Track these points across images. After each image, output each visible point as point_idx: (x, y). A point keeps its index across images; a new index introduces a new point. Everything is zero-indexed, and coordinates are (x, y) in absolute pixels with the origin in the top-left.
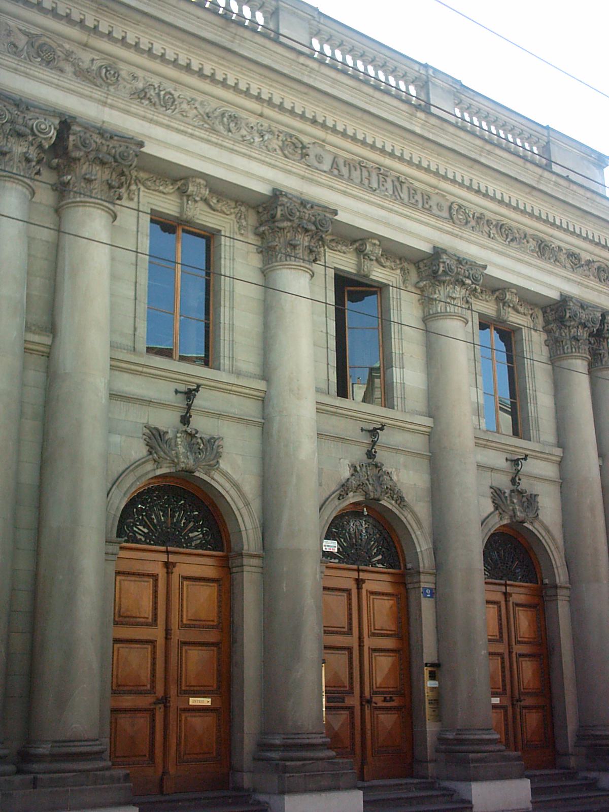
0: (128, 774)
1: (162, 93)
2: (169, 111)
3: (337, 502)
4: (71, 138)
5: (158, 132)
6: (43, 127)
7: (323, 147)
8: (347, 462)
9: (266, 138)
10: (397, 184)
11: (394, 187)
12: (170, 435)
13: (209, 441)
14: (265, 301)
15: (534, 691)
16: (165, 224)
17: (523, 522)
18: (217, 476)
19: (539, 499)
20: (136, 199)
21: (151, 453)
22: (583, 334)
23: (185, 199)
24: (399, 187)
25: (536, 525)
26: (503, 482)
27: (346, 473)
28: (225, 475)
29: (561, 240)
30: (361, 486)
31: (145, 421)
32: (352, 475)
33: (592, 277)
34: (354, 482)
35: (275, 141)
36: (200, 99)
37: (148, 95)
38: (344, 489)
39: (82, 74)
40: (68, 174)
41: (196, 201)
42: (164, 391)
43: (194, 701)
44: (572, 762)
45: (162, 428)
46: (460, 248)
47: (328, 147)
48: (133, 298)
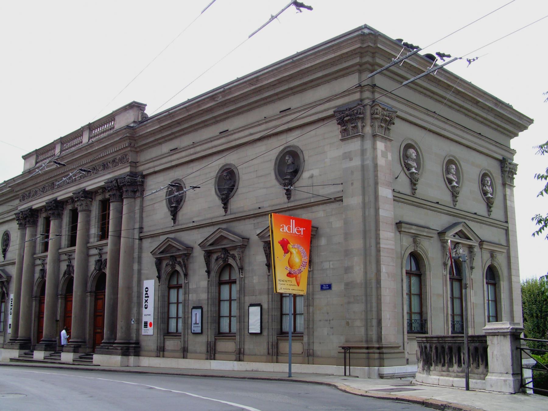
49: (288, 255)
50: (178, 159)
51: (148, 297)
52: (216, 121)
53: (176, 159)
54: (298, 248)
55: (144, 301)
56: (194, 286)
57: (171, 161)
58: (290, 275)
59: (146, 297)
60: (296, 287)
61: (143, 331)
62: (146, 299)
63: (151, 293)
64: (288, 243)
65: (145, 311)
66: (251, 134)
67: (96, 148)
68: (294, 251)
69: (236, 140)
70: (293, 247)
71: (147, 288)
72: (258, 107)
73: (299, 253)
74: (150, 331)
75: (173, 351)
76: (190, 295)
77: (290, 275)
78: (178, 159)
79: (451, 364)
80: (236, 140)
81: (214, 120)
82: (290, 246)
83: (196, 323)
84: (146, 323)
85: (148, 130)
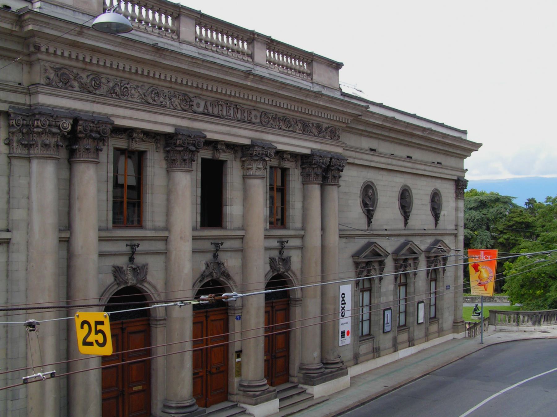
0: (54, 373)
1: (122, 88)
2: (125, 97)
3: (199, 284)
4: (79, 128)
5: (120, 112)
6: (65, 125)
7: (200, 98)
8: (204, 262)
9: (172, 100)
10: (235, 109)
11: (234, 111)
12: (125, 268)
13: (142, 267)
14: (168, 186)
15: (164, 53)
16: (119, 152)
17: (284, 273)
18: (146, 284)
19: (292, 259)
20: (106, 144)
21: (115, 280)
22: (319, 171)
23: (131, 140)
24: (236, 111)
25: (289, 272)
26: (275, 254)
27: (203, 268)
28: (150, 283)
29: (313, 120)
30: (211, 274)
31: (112, 264)
32: (206, 268)
33: (327, 137)
34: (207, 273)
35: (177, 100)
36: (140, 85)
37: (116, 91)
38: (203, 276)
39: (84, 88)
40: (77, 145)
41: (136, 141)
42: (122, 247)
43: (135, 389)
44: (295, 380)
45: (120, 266)
46: (264, 138)
47: (203, 97)
48: (106, 200)
49: (478, 273)
50: (377, 162)
51: (345, 303)
52: (409, 145)
53: (376, 161)
54: (486, 268)
55: (341, 309)
56: (384, 290)
57: (371, 161)
58: (480, 284)
59: (342, 304)
60: (485, 292)
61: (340, 342)
62: (343, 306)
63: (348, 299)
64: (478, 265)
65: (342, 321)
66: (425, 170)
67: (321, 103)
68: (483, 270)
69: (417, 169)
70: (482, 268)
71: (343, 294)
72: (429, 150)
73: (487, 271)
74: (348, 340)
75: (365, 354)
76: (382, 298)
77: (480, 284)
78: (377, 162)
79: (551, 320)
80: (417, 169)
81: (407, 143)
82: (480, 268)
83: (387, 323)
84: (343, 333)
85: (371, 120)
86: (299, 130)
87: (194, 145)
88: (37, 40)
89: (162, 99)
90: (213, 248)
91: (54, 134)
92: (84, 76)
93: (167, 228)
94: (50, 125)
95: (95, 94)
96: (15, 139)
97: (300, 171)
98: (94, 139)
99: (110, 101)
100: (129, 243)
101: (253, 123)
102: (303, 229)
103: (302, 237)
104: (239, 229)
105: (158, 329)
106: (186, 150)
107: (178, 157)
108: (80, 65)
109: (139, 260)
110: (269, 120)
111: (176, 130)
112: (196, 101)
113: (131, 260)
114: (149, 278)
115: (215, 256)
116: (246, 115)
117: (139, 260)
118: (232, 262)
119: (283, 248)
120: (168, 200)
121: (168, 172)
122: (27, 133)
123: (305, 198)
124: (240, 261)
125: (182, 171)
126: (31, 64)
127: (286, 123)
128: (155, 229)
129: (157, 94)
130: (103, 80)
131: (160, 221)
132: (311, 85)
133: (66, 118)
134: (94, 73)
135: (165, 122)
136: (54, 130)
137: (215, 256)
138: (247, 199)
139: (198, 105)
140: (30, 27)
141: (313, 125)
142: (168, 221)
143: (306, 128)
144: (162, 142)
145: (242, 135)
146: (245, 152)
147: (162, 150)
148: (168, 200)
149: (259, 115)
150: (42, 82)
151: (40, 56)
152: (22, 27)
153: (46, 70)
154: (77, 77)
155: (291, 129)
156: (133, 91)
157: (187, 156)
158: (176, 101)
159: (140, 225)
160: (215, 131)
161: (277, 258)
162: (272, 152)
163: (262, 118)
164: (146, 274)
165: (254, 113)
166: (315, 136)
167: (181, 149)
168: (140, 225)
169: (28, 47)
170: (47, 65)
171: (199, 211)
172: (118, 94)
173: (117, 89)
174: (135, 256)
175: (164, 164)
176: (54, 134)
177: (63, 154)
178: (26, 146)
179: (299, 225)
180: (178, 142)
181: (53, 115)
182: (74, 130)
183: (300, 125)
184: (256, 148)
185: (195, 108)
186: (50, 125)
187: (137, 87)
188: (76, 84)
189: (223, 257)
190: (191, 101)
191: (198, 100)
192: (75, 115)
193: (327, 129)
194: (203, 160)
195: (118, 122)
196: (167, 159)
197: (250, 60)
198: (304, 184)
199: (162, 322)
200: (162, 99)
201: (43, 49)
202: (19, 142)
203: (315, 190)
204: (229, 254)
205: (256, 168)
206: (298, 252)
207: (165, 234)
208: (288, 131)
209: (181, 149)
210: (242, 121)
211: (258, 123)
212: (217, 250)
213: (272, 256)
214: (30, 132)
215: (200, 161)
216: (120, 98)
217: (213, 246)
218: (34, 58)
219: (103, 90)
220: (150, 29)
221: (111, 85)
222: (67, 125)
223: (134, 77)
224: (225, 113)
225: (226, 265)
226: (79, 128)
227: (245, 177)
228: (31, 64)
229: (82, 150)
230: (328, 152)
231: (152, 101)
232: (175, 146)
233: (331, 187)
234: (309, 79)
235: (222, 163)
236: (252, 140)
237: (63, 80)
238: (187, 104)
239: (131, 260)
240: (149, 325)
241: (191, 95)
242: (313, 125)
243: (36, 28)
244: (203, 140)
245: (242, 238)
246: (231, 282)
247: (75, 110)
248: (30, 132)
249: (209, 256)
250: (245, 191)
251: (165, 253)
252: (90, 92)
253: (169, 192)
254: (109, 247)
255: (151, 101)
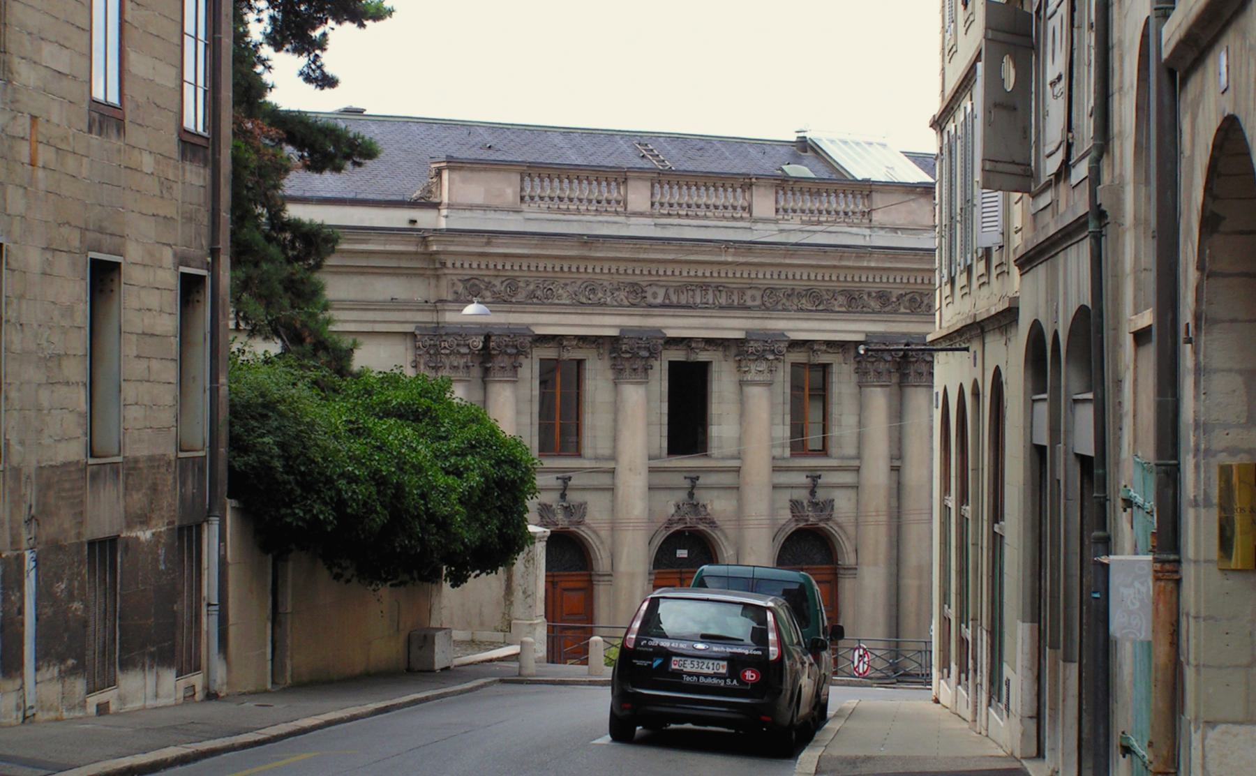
11: (715, 295)
28: (589, 528)
33: (902, 310)
34: (676, 518)
38: (670, 522)
42: (802, 479)
86: (841, 306)
87: (648, 349)
88: (442, 257)
89: (600, 295)
90: (687, 483)
91: (463, 355)
92: (497, 282)
93: (613, 458)
94: (458, 345)
95: (511, 302)
96: (422, 361)
97: (854, 366)
98: (510, 355)
99: (529, 308)
100: (560, 475)
101: (749, 308)
102: (859, 457)
103: (857, 470)
104: (733, 458)
105: (601, 587)
106: (635, 356)
107: (627, 365)
108: (492, 273)
109: (574, 497)
110: (773, 299)
111: (621, 331)
112: (650, 291)
113: (563, 496)
114: (587, 520)
115: (691, 495)
116: (735, 298)
117: (574, 497)
118: (718, 505)
119: (693, 487)
120: (615, 421)
121: (616, 384)
122: (435, 354)
123: (861, 408)
124: (735, 503)
125: (632, 383)
126: (438, 277)
127: (816, 301)
128: (596, 458)
129: (593, 291)
130: (521, 284)
131: (604, 448)
132: (867, 232)
133: (477, 335)
134: (509, 278)
135: (606, 324)
136: (464, 350)
137: (691, 495)
138: (748, 418)
139: (655, 295)
140: (435, 248)
141: (869, 294)
142: (615, 447)
143: (853, 302)
144: (607, 347)
145: (732, 326)
146: (737, 348)
147: (606, 357)
148: (615, 421)
149: (758, 294)
150: (450, 298)
151: (446, 271)
152: (426, 246)
153: (453, 284)
154: (489, 286)
155: (821, 307)
156: (560, 291)
157: (639, 364)
158: (622, 295)
159: (578, 454)
160: (677, 325)
161: (805, 503)
162: (783, 346)
163: (766, 298)
164: (584, 515)
165: (749, 293)
166: (874, 312)
167: (628, 355)
168: (578, 454)
169: (434, 262)
170: (454, 278)
171: (665, 433)
172: (542, 298)
173: (539, 293)
174: (695, 491)
175: (610, 375)
176: (463, 355)
177: (476, 372)
178: (433, 368)
179: (850, 450)
180: (624, 347)
181: (463, 332)
182: (486, 347)
183: (841, 299)
184: (752, 343)
185: (650, 300)
186: (458, 345)
187: (566, 285)
188: (488, 294)
189: (702, 497)
190: (643, 291)
191: (654, 289)
192: (485, 332)
193: (900, 297)
194: (670, 363)
195: (540, 331)
196: (614, 367)
197: (746, 215)
198: (860, 386)
199: (606, 578)
200: (600, 295)
201: (449, 264)
202: (426, 364)
203: (879, 400)
204: (715, 493)
205: (756, 370)
206: (852, 493)
207: (611, 465)
208: (817, 311)
209: (628, 355)
210: (730, 307)
211: (759, 307)
212: (693, 487)
213: (795, 497)
214: (437, 353)
215: (666, 366)
216: (543, 304)
217: (688, 481)
218: (440, 272)
219: (521, 296)
220: (583, 208)
221: (532, 287)
222: (478, 343)
223: (560, 275)
224: (698, 301)
225: (709, 507)
226: (492, 344)
227: (742, 383)
228: (438, 277)
229: (497, 367)
230: (904, 335)
231: (589, 299)
232: (625, 353)
233: (914, 389)
234: (866, 221)
235: (704, 368)
236: (747, 331)
237: (473, 291)
238: (637, 296)
239: (563, 496)
240: (591, 582)
241: (644, 284)
242: (869, 294)
243: (441, 248)
244: (662, 341)
245: (738, 470)
246: (719, 534)
247: (487, 325)
248: (437, 353)
249: (682, 496)
250: (742, 401)
251: (612, 489)
252: (505, 302)
253: (616, 408)
254: (783, 478)
255: (584, 300)
